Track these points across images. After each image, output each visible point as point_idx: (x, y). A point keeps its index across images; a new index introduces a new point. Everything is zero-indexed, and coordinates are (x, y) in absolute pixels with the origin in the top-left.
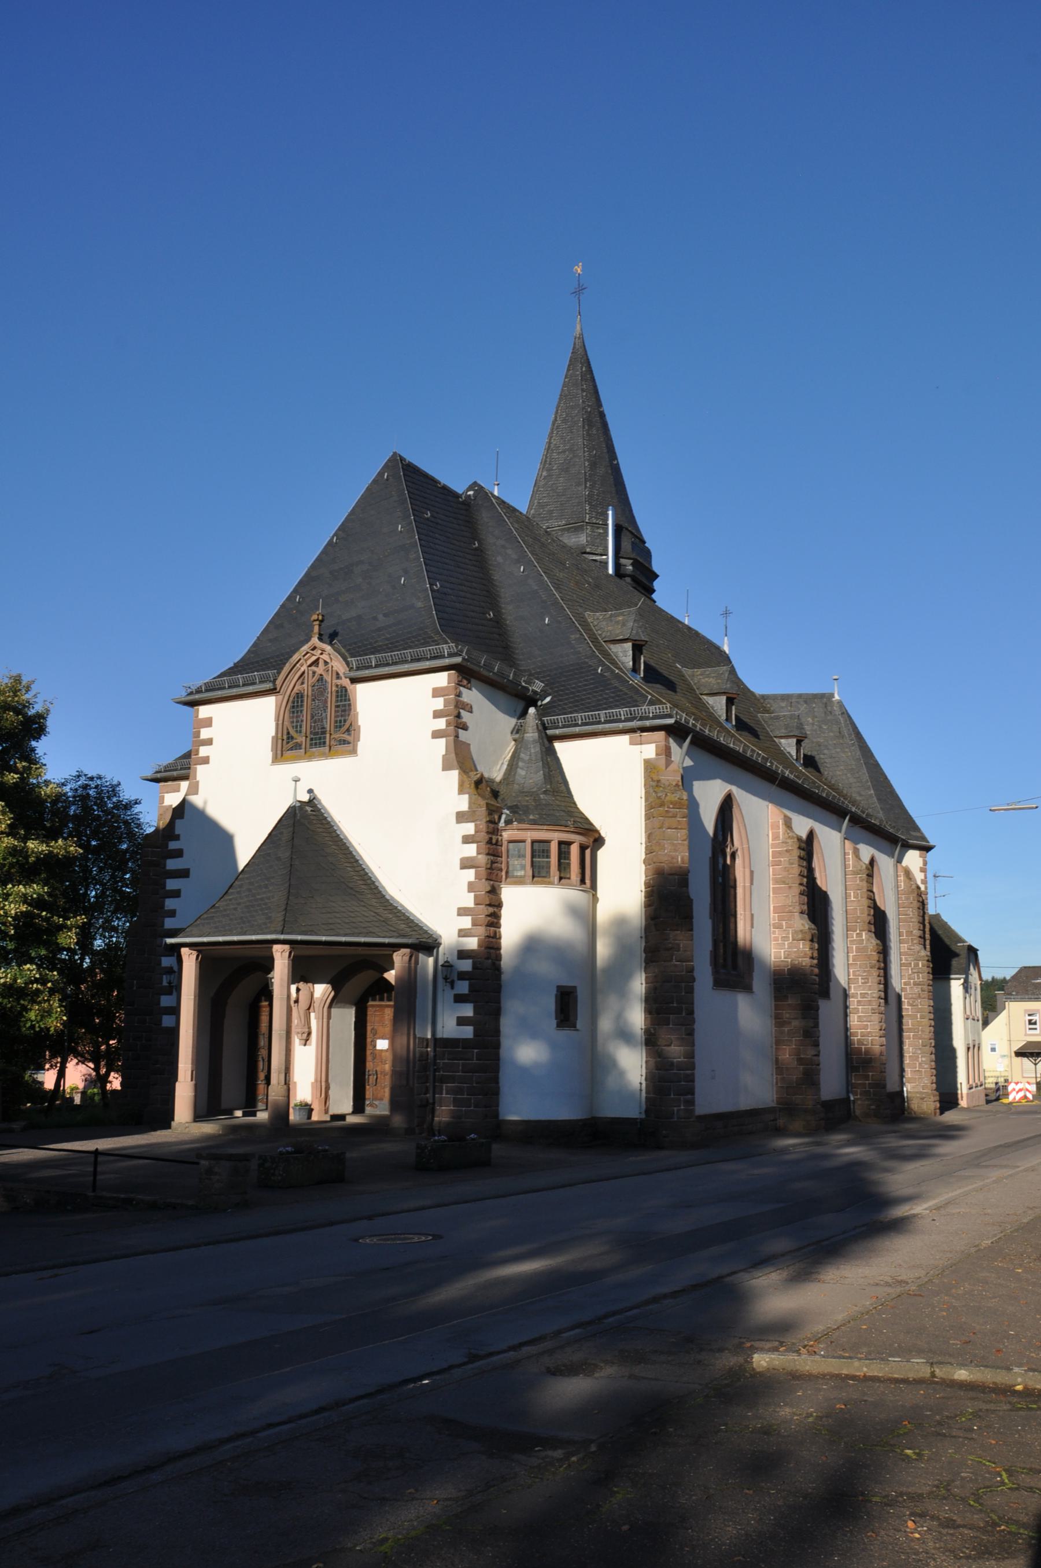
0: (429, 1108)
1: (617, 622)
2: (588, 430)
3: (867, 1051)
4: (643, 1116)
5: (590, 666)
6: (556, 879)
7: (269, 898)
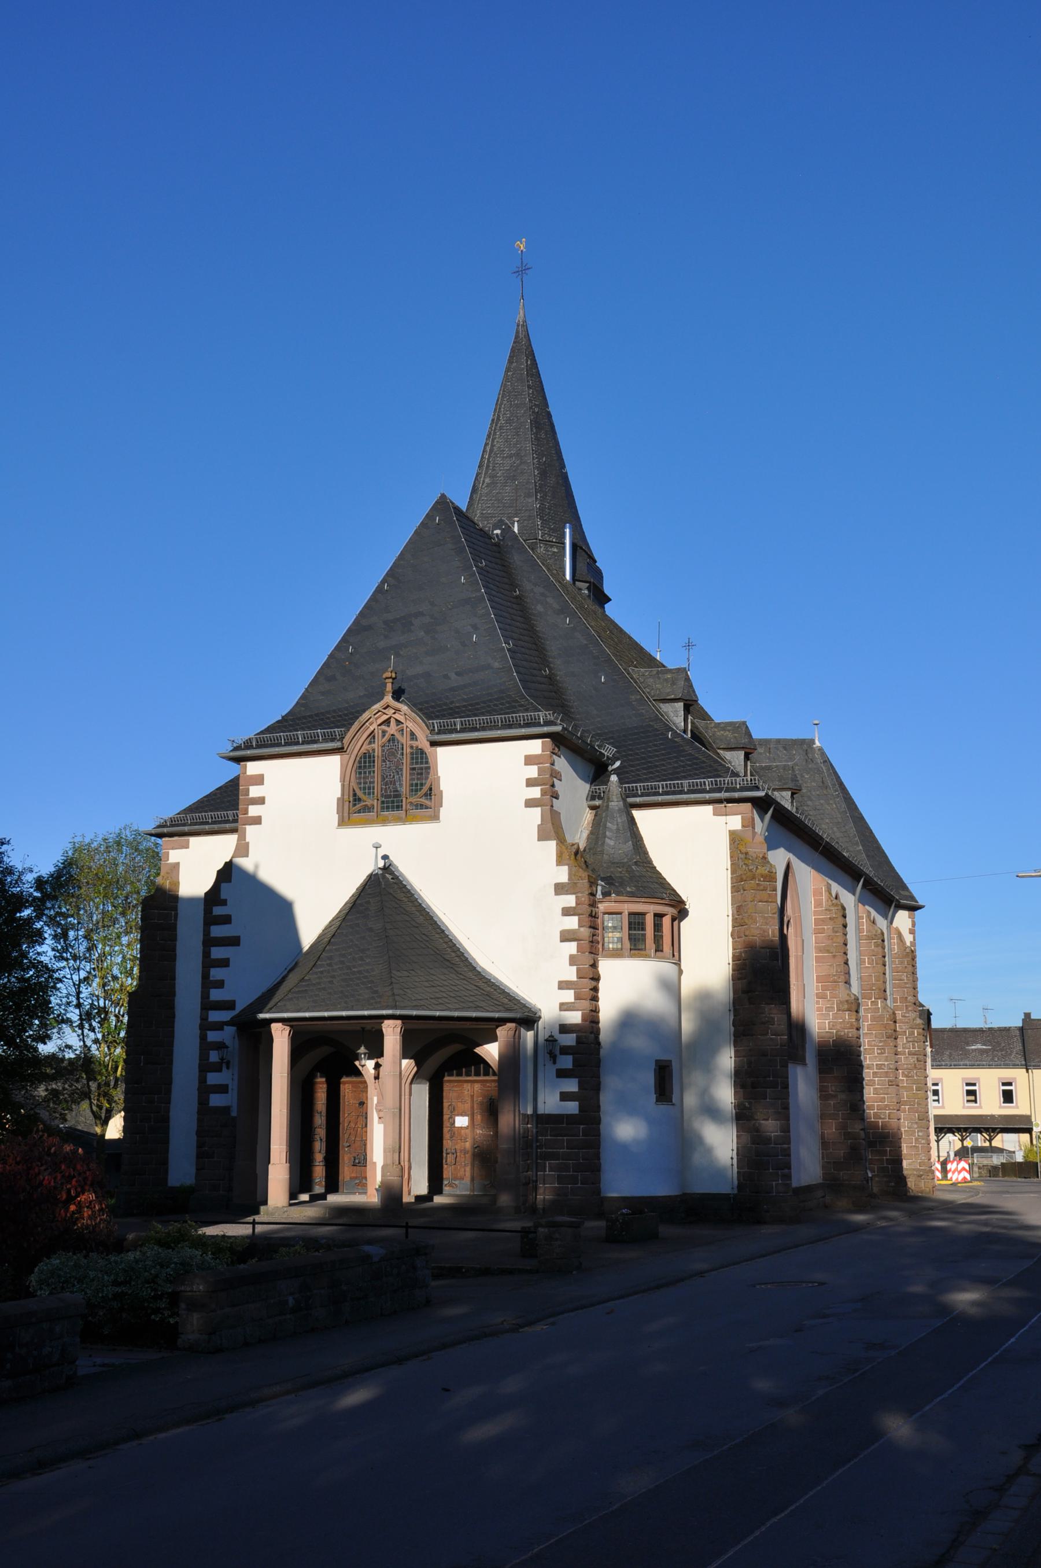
0: (531, 1185)
1: (666, 680)
2: (536, 433)
3: (884, 1126)
4: (736, 1191)
5: (657, 730)
6: (653, 951)
7: (367, 971)
